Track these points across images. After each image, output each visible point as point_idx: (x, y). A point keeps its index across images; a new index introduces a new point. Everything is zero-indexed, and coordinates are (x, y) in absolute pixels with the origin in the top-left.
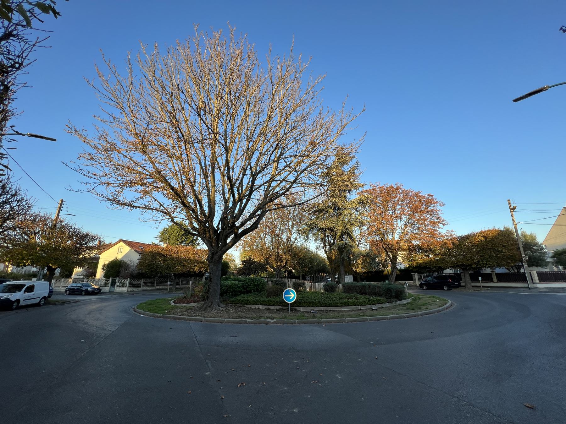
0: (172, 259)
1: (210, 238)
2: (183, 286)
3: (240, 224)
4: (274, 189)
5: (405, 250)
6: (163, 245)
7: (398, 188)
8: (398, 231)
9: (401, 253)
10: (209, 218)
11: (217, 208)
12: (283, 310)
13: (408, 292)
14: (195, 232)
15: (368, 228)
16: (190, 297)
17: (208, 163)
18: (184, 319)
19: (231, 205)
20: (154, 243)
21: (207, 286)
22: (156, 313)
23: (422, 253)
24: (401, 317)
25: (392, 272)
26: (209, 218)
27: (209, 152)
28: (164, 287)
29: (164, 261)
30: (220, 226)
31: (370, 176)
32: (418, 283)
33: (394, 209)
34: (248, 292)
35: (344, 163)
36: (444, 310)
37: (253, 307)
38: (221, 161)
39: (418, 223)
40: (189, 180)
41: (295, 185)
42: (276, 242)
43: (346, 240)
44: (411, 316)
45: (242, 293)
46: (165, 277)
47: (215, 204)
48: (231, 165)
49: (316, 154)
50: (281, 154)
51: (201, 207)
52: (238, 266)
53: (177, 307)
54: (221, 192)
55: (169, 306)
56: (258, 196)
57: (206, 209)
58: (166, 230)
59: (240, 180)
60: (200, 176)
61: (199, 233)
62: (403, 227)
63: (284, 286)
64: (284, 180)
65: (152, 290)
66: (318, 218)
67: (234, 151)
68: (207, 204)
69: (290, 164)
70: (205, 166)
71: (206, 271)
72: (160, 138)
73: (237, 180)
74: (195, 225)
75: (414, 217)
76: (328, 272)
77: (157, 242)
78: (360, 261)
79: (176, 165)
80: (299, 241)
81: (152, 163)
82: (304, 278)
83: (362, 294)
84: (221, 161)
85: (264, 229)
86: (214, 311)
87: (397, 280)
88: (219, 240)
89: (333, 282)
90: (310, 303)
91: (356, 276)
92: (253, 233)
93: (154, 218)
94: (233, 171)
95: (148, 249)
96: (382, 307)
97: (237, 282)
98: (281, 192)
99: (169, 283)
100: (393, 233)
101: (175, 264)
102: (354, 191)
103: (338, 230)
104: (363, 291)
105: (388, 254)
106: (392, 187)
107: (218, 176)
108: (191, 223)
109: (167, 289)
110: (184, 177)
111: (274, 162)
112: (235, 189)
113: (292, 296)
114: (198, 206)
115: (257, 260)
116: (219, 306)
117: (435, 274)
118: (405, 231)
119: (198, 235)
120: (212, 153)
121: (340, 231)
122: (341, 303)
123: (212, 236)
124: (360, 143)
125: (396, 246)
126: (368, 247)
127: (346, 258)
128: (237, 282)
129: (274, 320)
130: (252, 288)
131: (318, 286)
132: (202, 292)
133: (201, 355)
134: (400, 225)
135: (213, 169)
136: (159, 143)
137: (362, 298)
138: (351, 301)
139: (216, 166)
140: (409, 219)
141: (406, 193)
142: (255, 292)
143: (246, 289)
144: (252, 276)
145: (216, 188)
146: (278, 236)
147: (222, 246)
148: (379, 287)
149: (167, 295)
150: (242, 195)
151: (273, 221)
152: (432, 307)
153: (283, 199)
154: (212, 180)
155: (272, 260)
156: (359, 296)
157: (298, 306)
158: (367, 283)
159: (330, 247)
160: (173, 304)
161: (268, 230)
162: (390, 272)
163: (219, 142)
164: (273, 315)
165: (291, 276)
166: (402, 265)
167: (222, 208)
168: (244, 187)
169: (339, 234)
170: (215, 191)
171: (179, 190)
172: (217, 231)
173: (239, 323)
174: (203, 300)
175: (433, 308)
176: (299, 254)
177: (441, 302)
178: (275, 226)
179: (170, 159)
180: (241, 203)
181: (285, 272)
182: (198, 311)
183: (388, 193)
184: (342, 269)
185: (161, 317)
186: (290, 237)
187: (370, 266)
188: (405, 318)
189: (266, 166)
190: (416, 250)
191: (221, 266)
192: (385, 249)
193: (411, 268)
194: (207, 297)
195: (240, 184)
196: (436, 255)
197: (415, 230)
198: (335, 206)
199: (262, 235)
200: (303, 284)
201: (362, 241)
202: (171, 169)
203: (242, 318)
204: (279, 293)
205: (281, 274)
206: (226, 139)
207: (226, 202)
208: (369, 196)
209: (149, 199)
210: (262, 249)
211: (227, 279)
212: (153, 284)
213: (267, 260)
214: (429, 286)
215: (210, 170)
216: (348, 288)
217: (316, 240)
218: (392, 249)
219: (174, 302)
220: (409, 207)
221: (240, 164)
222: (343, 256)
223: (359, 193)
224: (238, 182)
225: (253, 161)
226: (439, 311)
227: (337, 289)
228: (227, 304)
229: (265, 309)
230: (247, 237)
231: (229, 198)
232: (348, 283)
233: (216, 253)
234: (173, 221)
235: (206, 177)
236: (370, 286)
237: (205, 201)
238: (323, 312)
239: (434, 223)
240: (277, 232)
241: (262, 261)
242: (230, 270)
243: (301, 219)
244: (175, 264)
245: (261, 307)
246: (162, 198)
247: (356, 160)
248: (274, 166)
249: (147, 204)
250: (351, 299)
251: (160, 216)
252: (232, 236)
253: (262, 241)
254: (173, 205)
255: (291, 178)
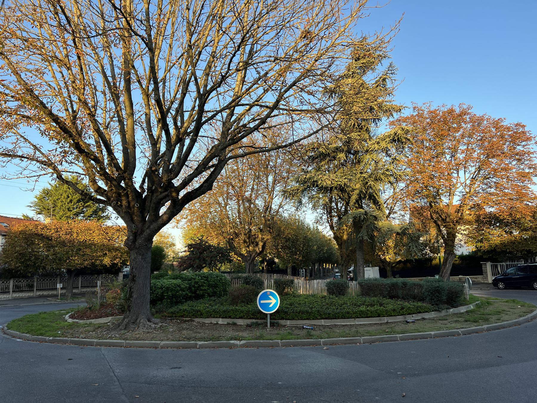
0: (63, 244)
1: (129, 207)
2: (85, 290)
3: (181, 181)
4: (239, 119)
5: (469, 223)
6: (44, 220)
7: (463, 113)
8: (459, 191)
9: (463, 228)
10: (125, 172)
11: (138, 154)
12: (257, 325)
13: (470, 292)
14: (99, 197)
15: (407, 186)
16: (98, 308)
17: (117, 71)
18: (91, 344)
19: (163, 148)
20: (27, 217)
21: (127, 289)
22: (41, 334)
23: (500, 227)
24: (453, 334)
25: (446, 260)
26: (125, 172)
27: (118, 52)
28: (51, 293)
29: (49, 247)
30: (146, 186)
31: (413, 94)
32: (490, 279)
33: (454, 152)
34: (198, 297)
35: (365, 68)
36: (527, 321)
37: (207, 321)
38: (142, 66)
39: (495, 176)
40: (85, 103)
41: (276, 112)
42: (245, 210)
43: (368, 207)
44: (470, 333)
45: (187, 298)
46: (50, 276)
47: (135, 148)
48: (160, 75)
49: (314, 53)
50: (251, 54)
51: (110, 152)
52: (181, 255)
53: (77, 325)
54: (144, 125)
55: (63, 324)
56: (211, 133)
57: (119, 156)
58: (47, 193)
59: (177, 102)
60: (105, 95)
61: (109, 199)
62: (468, 182)
63: (260, 285)
64: (256, 103)
65: (30, 298)
66: (318, 169)
67: (165, 47)
68: (121, 148)
69: (267, 73)
70: (114, 77)
71: (124, 264)
72: (27, 25)
73: (172, 103)
74: (102, 184)
75: (489, 164)
76: (337, 262)
77: (31, 214)
78: (391, 243)
79: (59, 76)
80: (288, 210)
81: (16, 73)
82: (295, 273)
83: (391, 297)
84: (142, 66)
85: (225, 189)
86: (141, 330)
87: (452, 274)
88: (146, 210)
89: (344, 279)
90: (303, 313)
91: (385, 269)
92: (206, 197)
93: (26, 172)
94: (164, 88)
95: (17, 228)
96: (424, 319)
97: (178, 281)
98: (252, 125)
99: (59, 286)
100: (451, 194)
101: (67, 253)
102: (384, 119)
103: (353, 190)
104: (392, 293)
105: (440, 231)
106: (451, 112)
107: (137, 96)
108: (93, 181)
109: (56, 296)
110: (75, 98)
111: (238, 70)
112: (170, 121)
113: (273, 302)
114: (105, 152)
115: (214, 242)
116: (149, 321)
117: (522, 263)
118: (472, 190)
119: (108, 203)
120: (124, 54)
121: (357, 192)
122: (356, 313)
123: (132, 204)
124: (392, 34)
125: (454, 216)
126: (407, 217)
127: (366, 238)
128: (178, 281)
129: (243, 342)
130: (205, 290)
131: (318, 286)
132: (120, 299)
133: (123, 397)
134: (462, 180)
135: (128, 82)
136: (25, 34)
137: (391, 304)
138: (372, 309)
139: (133, 77)
140: (479, 169)
141: (477, 122)
142: (210, 296)
143: (195, 292)
144: (205, 270)
145: (136, 117)
146: (249, 201)
147: (151, 221)
148: (420, 286)
149: (58, 306)
150: (182, 130)
151: (239, 175)
152: (505, 317)
153: (257, 136)
154: (127, 103)
155: (238, 242)
156: (386, 301)
157: (283, 319)
158: (401, 280)
159: (340, 218)
160: (70, 320)
161: (231, 191)
162: (442, 260)
163: (136, 34)
164: (241, 334)
165: (272, 268)
166: (464, 247)
167: (147, 154)
168: (186, 115)
169: (354, 197)
170: (134, 122)
171: (68, 123)
172: (140, 194)
173: (185, 347)
174: (122, 310)
175: (508, 320)
176: (287, 232)
177: (524, 309)
178: (244, 184)
179: (47, 63)
180: (183, 145)
181: (262, 262)
182: (113, 329)
183: (445, 122)
184: (359, 256)
185: (50, 341)
186: (271, 202)
187: (408, 251)
188: (459, 334)
189: (224, 78)
190: (491, 222)
191: (150, 254)
192: (435, 222)
193: (479, 254)
194: (129, 306)
195: (177, 111)
196: (526, 230)
197: (491, 187)
198: (348, 148)
199: (220, 199)
200: (292, 282)
201: (396, 209)
202: (50, 82)
203: (189, 339)
204: (250, 297)
205: (255, 265)
206: (149, 29)
207: (154, 143)
208: (410, 127)
209: (13, 139)
210: (222, 225)
211: (161, 276)
212: (30, 288)
213: (230, 242)
214: (509, 283)
215: (123, 83)
216: (368, 288)
217: (314, 207)
218: (446, 222)
219: (72, 317)
220: (481, 147)
221: (176, 72)
222: (361, 235)
223: (392, 123)
224: (175, 106)
225: (202, 65)
226: (519, 324)
227: (350, 290)
228: (164, 318)
229: (228, 324)
230: (195, 204)
231: (159, 136)
232: (369, 280)
233: (142, 233)
234: (60, 177)
235: (116, 97)
236: (405, 284)
237: (116, 140)
238: (324, 327)
239: (524, 176)
240: (247, 194)
241: (222, 245)
242: (166, 262)
243: (288, 172)
244: (67, 253)
245: (221, 321)
246: (38, 137)
247: (390, 61)
248: (240, 75)
249: (11, 147)
250: (372, 305)
251: (35, 168)
252: (168, 204)
253: (221, 211)
254: (59, 150)
255: (270, 99)
